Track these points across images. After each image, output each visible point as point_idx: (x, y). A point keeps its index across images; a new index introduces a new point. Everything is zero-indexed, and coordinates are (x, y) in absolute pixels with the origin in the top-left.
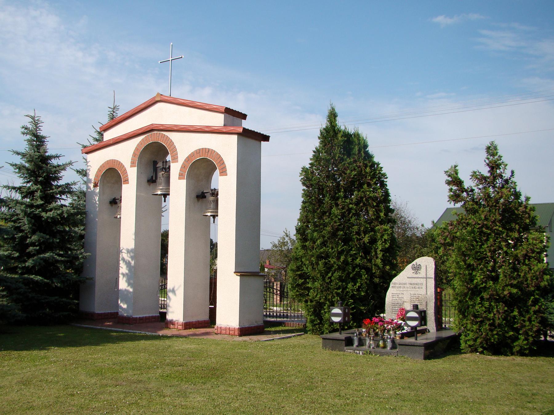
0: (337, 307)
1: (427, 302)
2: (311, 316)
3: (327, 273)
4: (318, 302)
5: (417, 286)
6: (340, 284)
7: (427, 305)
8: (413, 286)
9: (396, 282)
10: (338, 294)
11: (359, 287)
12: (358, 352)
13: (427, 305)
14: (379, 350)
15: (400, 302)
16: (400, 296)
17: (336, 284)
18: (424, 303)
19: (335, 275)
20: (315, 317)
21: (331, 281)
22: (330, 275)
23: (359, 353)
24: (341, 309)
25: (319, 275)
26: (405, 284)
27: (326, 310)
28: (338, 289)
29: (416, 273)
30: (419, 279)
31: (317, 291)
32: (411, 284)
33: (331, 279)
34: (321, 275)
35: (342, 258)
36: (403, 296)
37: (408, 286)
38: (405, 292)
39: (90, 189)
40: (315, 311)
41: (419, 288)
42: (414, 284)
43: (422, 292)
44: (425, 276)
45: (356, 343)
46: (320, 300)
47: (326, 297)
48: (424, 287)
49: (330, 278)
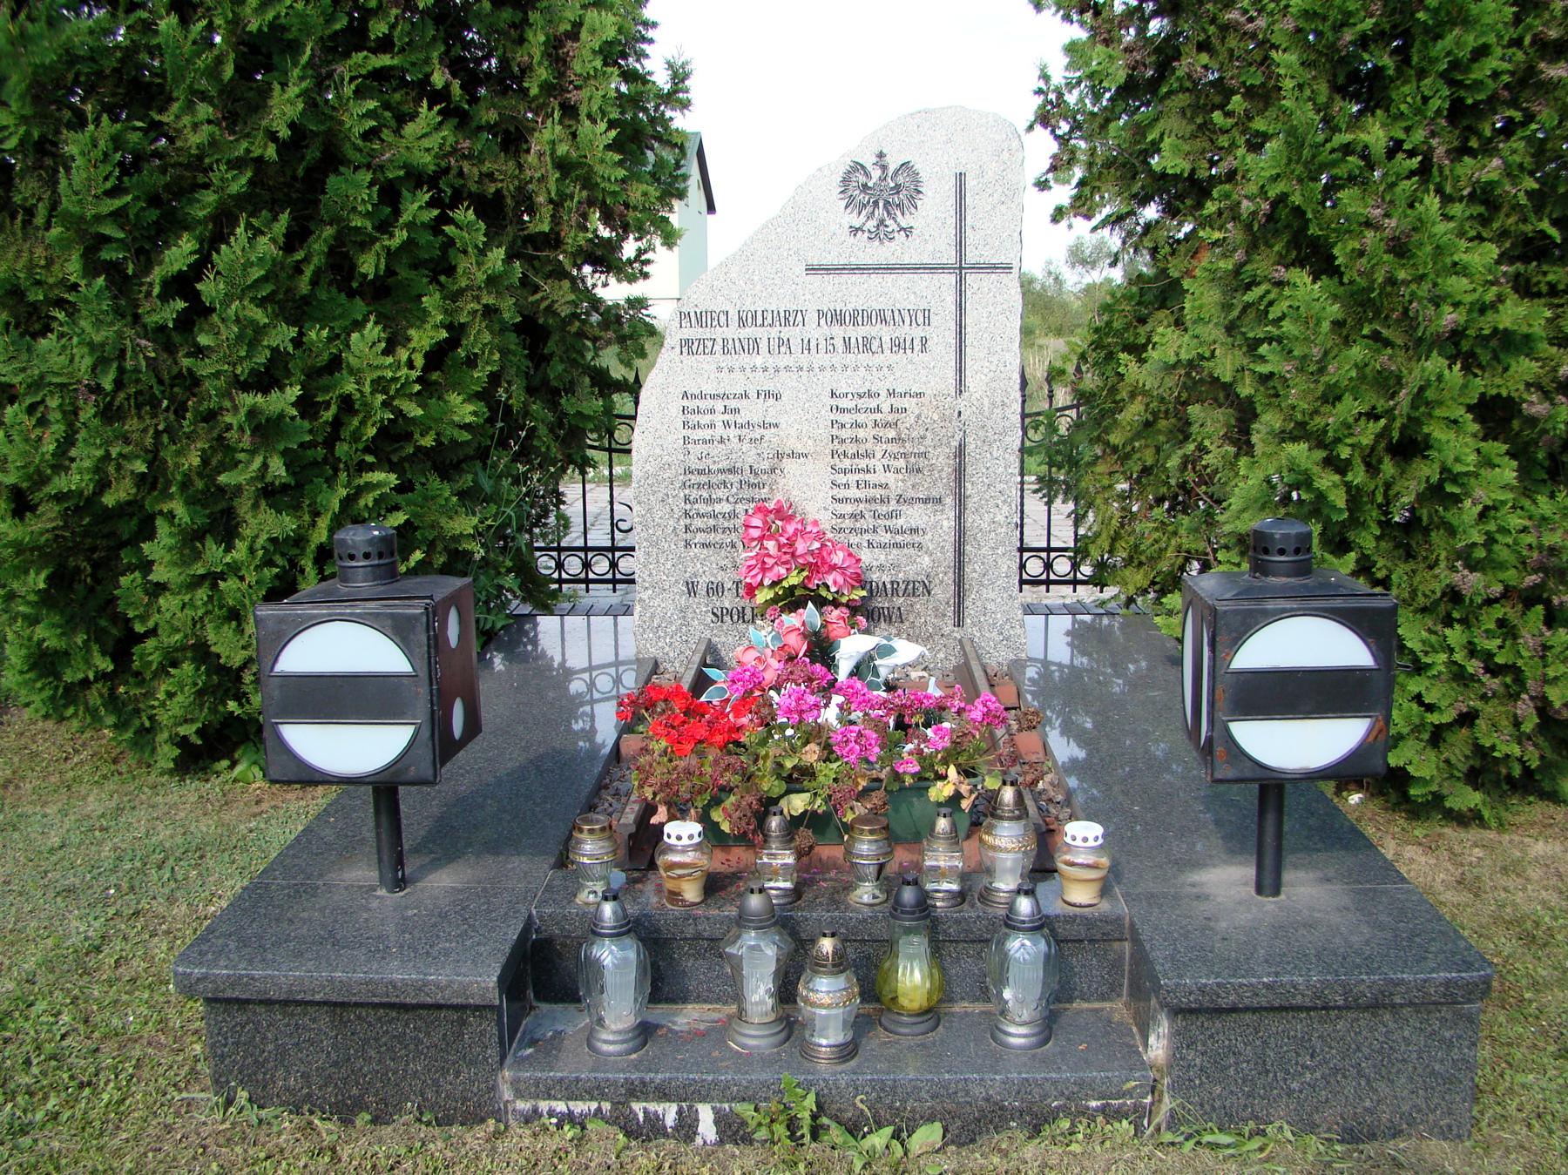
0: (339, 606)
1: (961, 452)
2: (33, 621)
3: (147, 251)
4: (81, 506)
5: (886, 333)
6: (282, 335)
7: (960, 473)
8: (855, 333)
9: (718, 305)
10: (266, 429)
11: (437, 357)
12: (669, 1113)
13: (960, 473)
14: (906, 1065)
15: (748, 456)
16: (752, 411)
17: (252, 335)
18: (942, 460)
19: (224, 256)
20: (69, 627)
21: (198, 311)
22: (180, 254)
23: (687, 1128)
24: (399, 631)
25: (73, 267)
26: (787, 319)
27: (159, 574)
28: (266, 380)
29: (880, 234)
30: (904, 279)
31: (71, 414)
32: (838, 318)
33: (194, 297)
34: (92, 267)
35: (285, 106)
36: (772, 410)
37: (815, 331)
38: (786, 383)
39: (188, 355)
40: (61, 579)
41: (898, 345)
42: (856, 318)
43: (928, 372)
44: (972, 257)
45: (619, 1008)
46: (103, 485)
47: (154, 458)
48: (942, 334)
49: (182, 285)
